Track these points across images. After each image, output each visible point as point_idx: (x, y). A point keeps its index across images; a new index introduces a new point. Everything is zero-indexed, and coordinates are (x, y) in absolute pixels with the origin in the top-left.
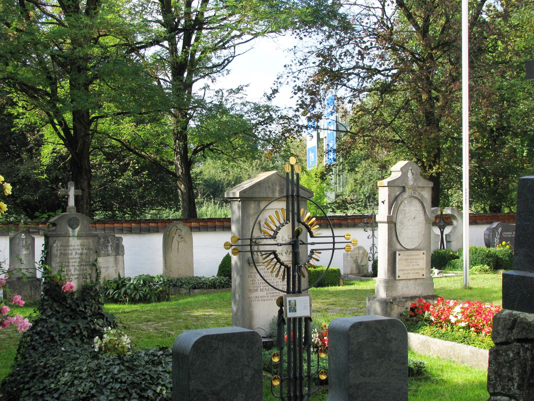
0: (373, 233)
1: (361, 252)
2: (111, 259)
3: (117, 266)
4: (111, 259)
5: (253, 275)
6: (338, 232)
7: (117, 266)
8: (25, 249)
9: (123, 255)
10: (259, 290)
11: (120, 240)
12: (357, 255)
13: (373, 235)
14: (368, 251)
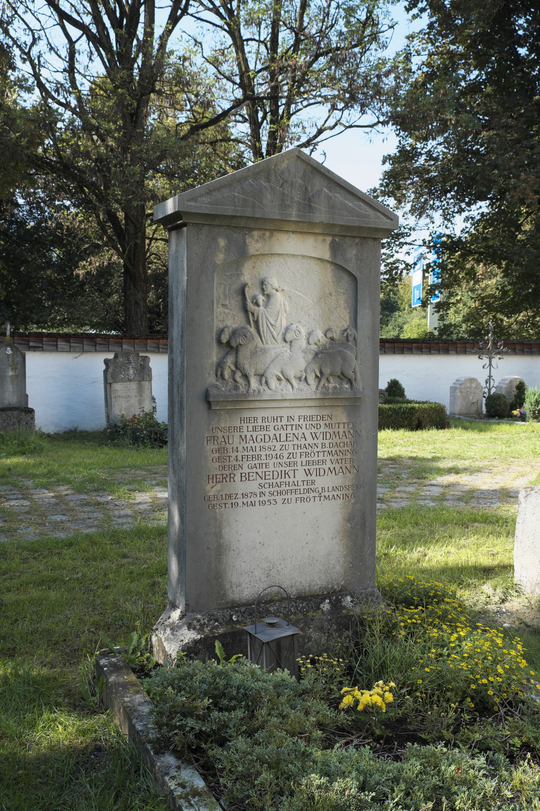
0: (490, 361)
1: (474, 385)
2: (133, 386)
3: (141, 396)
4: (133, 386)
5: (220, 434)
6: (233, 49)
7: (141, 396)
8: (12, 369)
9: (151, 380)
10: (237, 478)
11: (146, 359)
12: (468, 390)
13: (490, 365)
14: (483, 384)
